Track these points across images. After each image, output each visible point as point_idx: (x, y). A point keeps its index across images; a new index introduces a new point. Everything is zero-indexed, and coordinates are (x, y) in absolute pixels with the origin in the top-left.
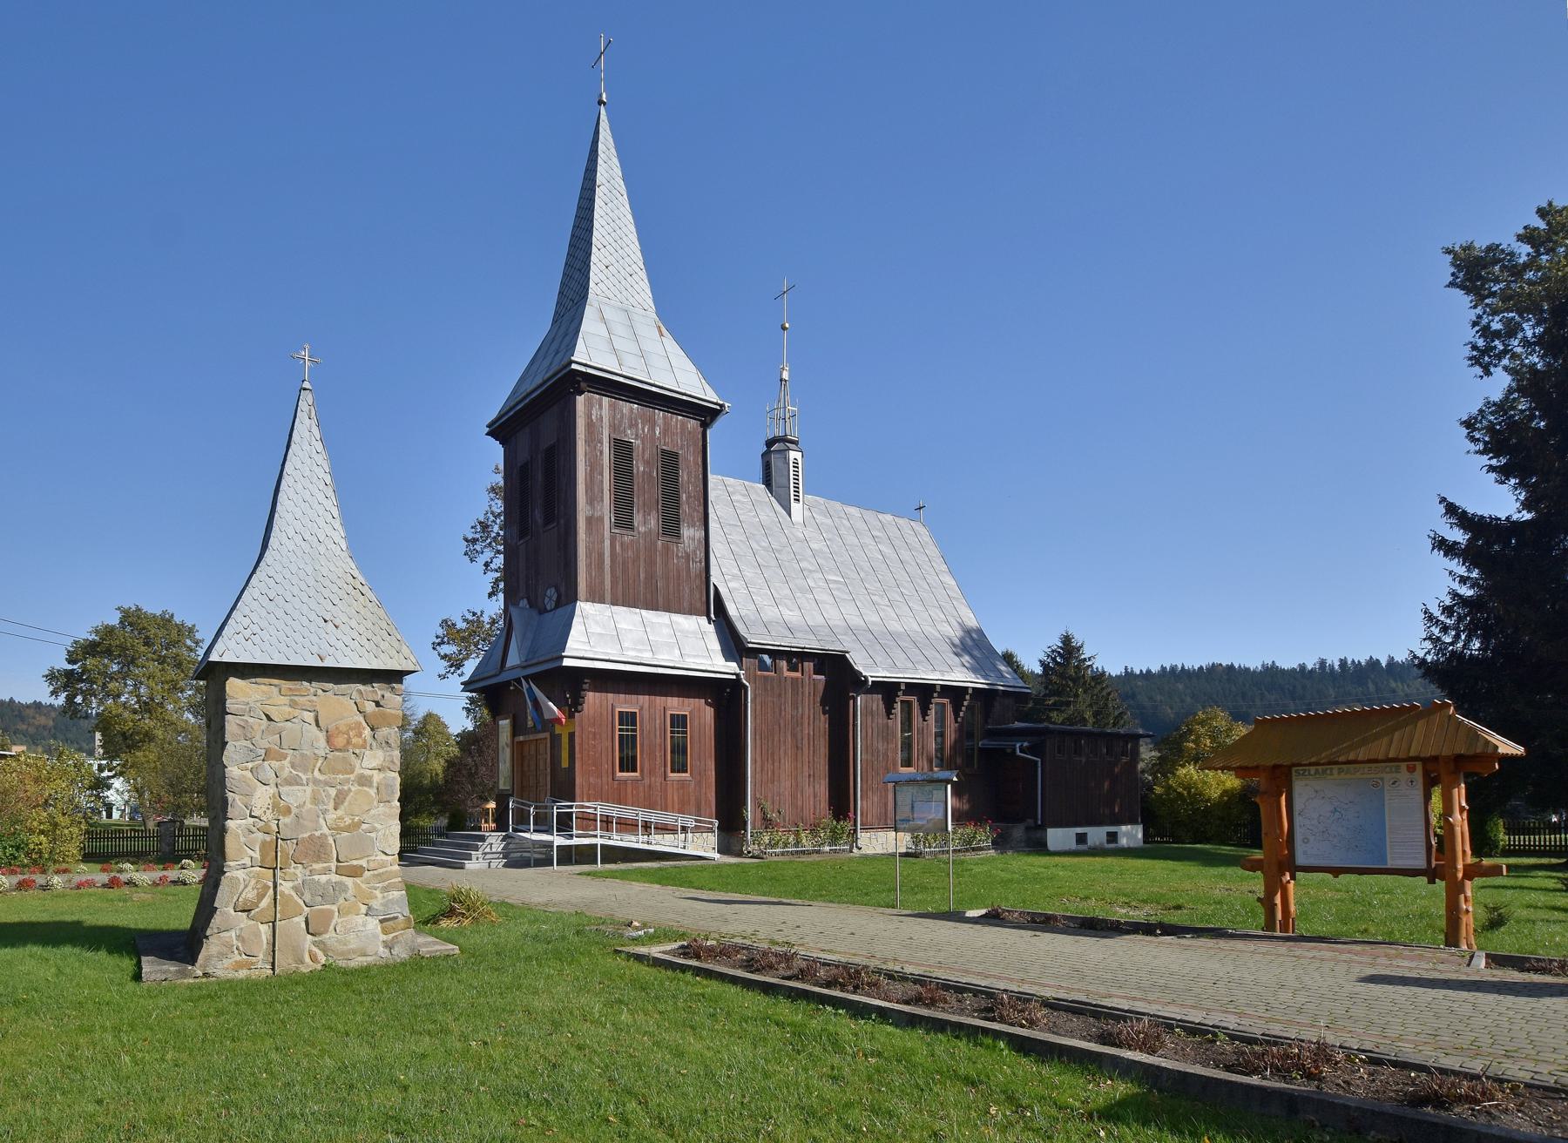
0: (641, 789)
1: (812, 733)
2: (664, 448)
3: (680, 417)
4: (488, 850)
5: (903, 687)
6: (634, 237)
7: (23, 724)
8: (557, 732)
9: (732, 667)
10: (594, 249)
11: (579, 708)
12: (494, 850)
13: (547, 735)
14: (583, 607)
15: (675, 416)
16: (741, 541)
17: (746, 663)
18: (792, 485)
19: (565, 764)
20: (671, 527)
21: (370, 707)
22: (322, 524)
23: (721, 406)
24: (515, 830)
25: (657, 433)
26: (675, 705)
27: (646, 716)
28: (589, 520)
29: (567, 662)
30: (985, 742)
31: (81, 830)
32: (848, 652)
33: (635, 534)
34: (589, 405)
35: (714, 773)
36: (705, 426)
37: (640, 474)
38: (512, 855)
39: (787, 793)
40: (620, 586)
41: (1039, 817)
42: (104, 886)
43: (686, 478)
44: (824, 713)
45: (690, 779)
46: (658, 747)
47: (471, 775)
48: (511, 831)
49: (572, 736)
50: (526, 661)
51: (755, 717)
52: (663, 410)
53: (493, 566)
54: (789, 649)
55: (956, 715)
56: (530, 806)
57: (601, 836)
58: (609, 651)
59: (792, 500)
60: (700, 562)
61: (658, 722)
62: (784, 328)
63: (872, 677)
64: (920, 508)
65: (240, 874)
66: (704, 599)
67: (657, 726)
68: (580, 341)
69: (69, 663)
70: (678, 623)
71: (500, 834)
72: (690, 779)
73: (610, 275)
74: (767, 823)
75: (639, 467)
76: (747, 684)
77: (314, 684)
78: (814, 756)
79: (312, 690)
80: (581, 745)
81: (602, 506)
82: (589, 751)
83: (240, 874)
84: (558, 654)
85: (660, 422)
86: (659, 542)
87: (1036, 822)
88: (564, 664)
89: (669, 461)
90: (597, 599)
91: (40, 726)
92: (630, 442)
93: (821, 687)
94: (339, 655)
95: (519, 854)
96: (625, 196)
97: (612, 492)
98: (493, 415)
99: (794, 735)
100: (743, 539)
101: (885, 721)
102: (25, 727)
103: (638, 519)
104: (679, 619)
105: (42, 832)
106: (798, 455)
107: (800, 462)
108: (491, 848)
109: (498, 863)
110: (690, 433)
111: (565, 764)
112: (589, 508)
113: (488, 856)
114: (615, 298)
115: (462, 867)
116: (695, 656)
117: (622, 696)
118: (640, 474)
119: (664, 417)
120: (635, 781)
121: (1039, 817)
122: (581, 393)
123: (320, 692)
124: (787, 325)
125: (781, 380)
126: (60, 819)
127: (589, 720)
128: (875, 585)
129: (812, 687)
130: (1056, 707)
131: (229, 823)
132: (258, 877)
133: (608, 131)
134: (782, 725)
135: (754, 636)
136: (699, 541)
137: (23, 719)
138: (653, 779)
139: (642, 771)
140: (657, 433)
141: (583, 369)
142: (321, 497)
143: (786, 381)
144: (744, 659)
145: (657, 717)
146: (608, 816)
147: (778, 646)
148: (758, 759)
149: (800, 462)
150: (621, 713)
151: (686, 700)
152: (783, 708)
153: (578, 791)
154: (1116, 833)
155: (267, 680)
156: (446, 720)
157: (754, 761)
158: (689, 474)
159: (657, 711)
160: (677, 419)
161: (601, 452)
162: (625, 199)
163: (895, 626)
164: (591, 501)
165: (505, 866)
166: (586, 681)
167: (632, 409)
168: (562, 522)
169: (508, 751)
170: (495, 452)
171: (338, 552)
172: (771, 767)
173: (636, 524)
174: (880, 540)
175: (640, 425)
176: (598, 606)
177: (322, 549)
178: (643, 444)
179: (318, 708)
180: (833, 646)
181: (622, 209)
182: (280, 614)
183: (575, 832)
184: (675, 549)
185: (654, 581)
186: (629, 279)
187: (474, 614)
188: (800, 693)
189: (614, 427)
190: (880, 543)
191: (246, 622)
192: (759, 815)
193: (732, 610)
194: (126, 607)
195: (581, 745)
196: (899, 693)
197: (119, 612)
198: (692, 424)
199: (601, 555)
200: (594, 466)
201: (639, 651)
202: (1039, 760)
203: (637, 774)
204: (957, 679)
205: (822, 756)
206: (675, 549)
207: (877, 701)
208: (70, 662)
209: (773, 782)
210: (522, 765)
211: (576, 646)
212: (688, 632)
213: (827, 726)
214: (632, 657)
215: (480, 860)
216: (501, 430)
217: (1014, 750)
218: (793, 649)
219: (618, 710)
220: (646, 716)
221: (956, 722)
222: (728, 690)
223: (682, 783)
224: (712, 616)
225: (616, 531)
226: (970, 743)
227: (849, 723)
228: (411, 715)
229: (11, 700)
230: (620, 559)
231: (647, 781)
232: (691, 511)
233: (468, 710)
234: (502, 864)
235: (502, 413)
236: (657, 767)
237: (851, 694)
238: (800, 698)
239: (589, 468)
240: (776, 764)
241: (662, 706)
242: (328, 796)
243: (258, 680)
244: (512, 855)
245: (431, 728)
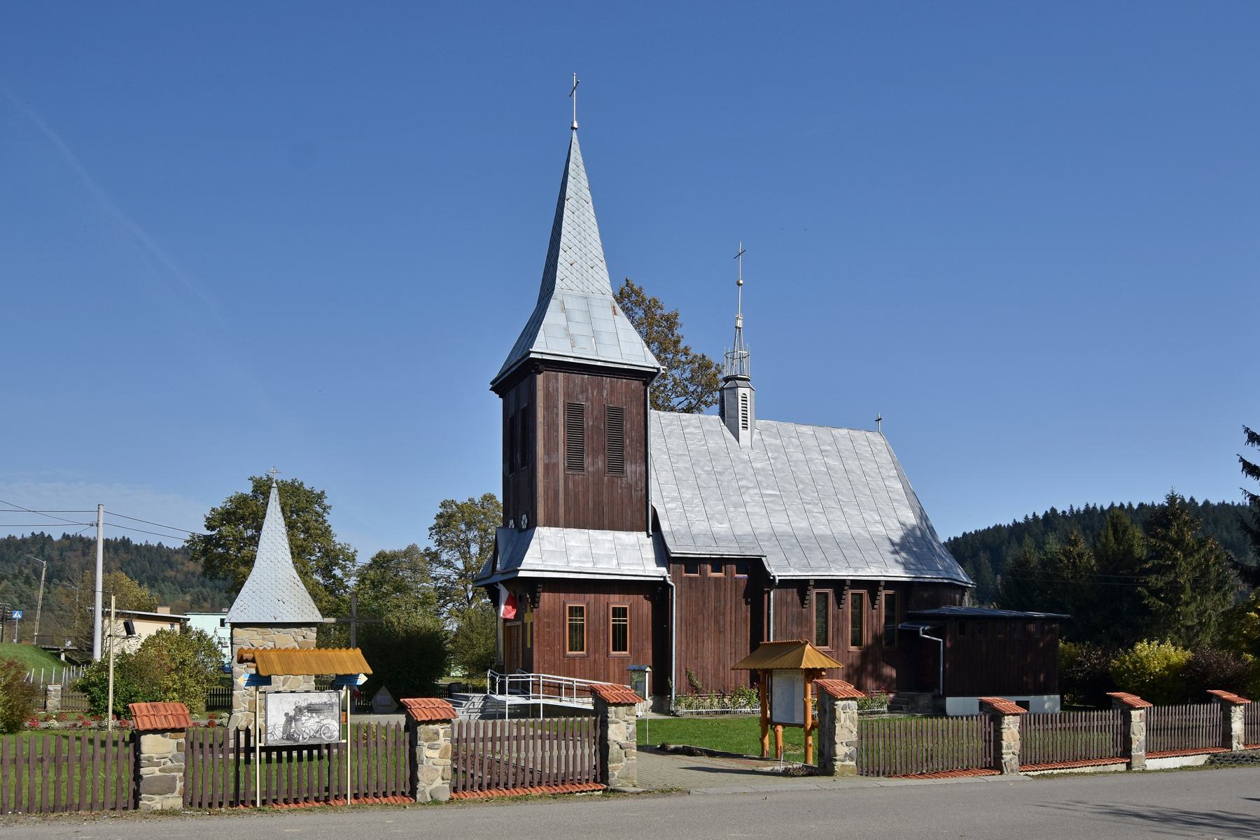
0: (587, 663)
1: (733, 619)
2: (610, 405)
3: (624, 380)
5: (812, 583)
6: (596, 236)
7: (172, 570)
10: (561, 252)
11: (536, 605)
12: (476, 707)
14: (541, 531)
15: (620, 380)
16: (686, 468)
17: (673, 568)
18: (740, 415)
19: (529, 646)
20: (616, 467)
21: (300, 639)
22: (279, 552)
23: (658, 369)
25: (605, 395)
26: (616, 601)
27: (592, 609)
28: (547, 467)
29: (521, 574)
30: (904, 624)
31: (203, 688)
32: (765, 556)
34: (547, 380)
35: (650, 652)
36: (646, 384)
37: (590, 427)
39: (709, 666)
40: (572, 514)
41: (941, 688)
42: (205, 726)
43: (629, 426)
44: (747, 603)
45: (629, 655)
46: (601, 632)
50: (505, 569)
51: (680, 608)
52: (610, 377)
54: (709, 556)
57: (543, 698)
58: (557, 564)
59: (740, 428)
60: (641, 490)
61: (602, 613)
62: (739, 284)
63: (778, 576)
64: (879, 420)
65: (239, 715)
66: (644, 518)
67: (601, 616)
68: (541, 332)
69: (208, 529)
70: (620, 539)
71: (480, 695)
72: (629, 655)
73: (574, 271)
74: (694, 689)
75: (589, 422)
76: (673, 584)
77: (273, 629)
78: (735, 638)
79: (273, 632)
81: (558, 455)
83: (239, 715)
84: (515, 568)
85: (608, 386)
86: (606, 478)
88: (519, 575)
89: (615, 416)
90: (553, 524)
91: (188, 572)
93: (743, 585)
94: (284, 617)
96: (591, 203)
97: (566, 444)
98: (495, 375)
99: (717, 622)
100: (688, 466)
101: (799, 609)
102: (173, 573)
103: (587, 461)
104: (622, 535)
105: (175, 690)
106: (747, 391)
110: (633, 391)
111: (529, 646)
112: (546, 457)
114: (577, 289)
116: (629, 564)
117: (572, 595)
118: (590, 427)
119: (611, 382)
120: (582, 657)
121: (941, 688)
122: (540, 373)
123: (276, 633)
124: (741, 282)
125: (736, 327)
126: (187, 680)
127: (544, 614)
128: (812, 494)
129: (734, 584)
130: (1157, 570)
131: (234, 692)
132: (247, 715)
133: (579, 152)
134: (706, 615)
135: (675, 549)
136: (641, 474)
137: (171, 566)
138: (597, 656)
139: (588, 650)
140: (605, 395)
141: (539, 356)
142: (280, 540)
143: (740, 328)
144: (671, 565)
145: (601, 610)
147: (699, 554)
148: (684, 640)
150: (571, 608)
151: (626, 596)
152: (706, 601)
153: (535, 665)
154: (1028, 702)
155: (250, 628)
157: (679, 643)
158: (632, 424)
159: (601, 605)
160: (622, 383)
161: (557, 415)
162: (590, 208)
163: (821, 529)
164: (548, 452)
166: (539, 586)
167: (583, 379)
168: (530, 466)
170: (497, 402)
171: (288, 565)
173: (585, 466)
174: (827, 453)
175: (590, 391)
176: (553, 529)
177: (280, 565)
178: (592, 404)
179: (275, 640)
181: (587, 214)
182: (257, 598)
183: (531, 694)
184: (619, 482)
185: (601, 508)
186: (590, 271)
188: (723, 589)
189: (567, 394)
190: (827, 456)
191: (242, 603)
192: (685, 680)
193: (664, 526)
194: (258, 477)
195: (538, 632)
196: (809, 588)
197: (251, 481)
198: (636, 384)
199: (556, 492)
200: (551, 426)
201: (583, 562)
202: (941, 640)
203: (584, 653)
204: (868, 574)
206: (619, 482)
207: (792, 595)
208: (209, 527)
209: (697, 658)
210: (511, 644)
212: (627, 545)
213: (749, 614)
214: (575, 568)
215: (465, 713)
216: (500, 387)
217: (918, 632)
218: (712, 556)
219: (568, 605)
220: (592, 609)
223: (622, 659)
224: (650, 531)
225: (569, 473)
226: (893, 625)
227: (764, 612)
229: (160, 545)
230: (572, 493)
231: (592, 658)
232: (633, 451)
234: (478, 717)
235: (503, 371)
236: (601, 647)
237: (765, 589)
238: (722, 594)
239: (546, 428)
240: (700, 644)
241: (606, 601)
242: (280, 680)
243: (248, 629)
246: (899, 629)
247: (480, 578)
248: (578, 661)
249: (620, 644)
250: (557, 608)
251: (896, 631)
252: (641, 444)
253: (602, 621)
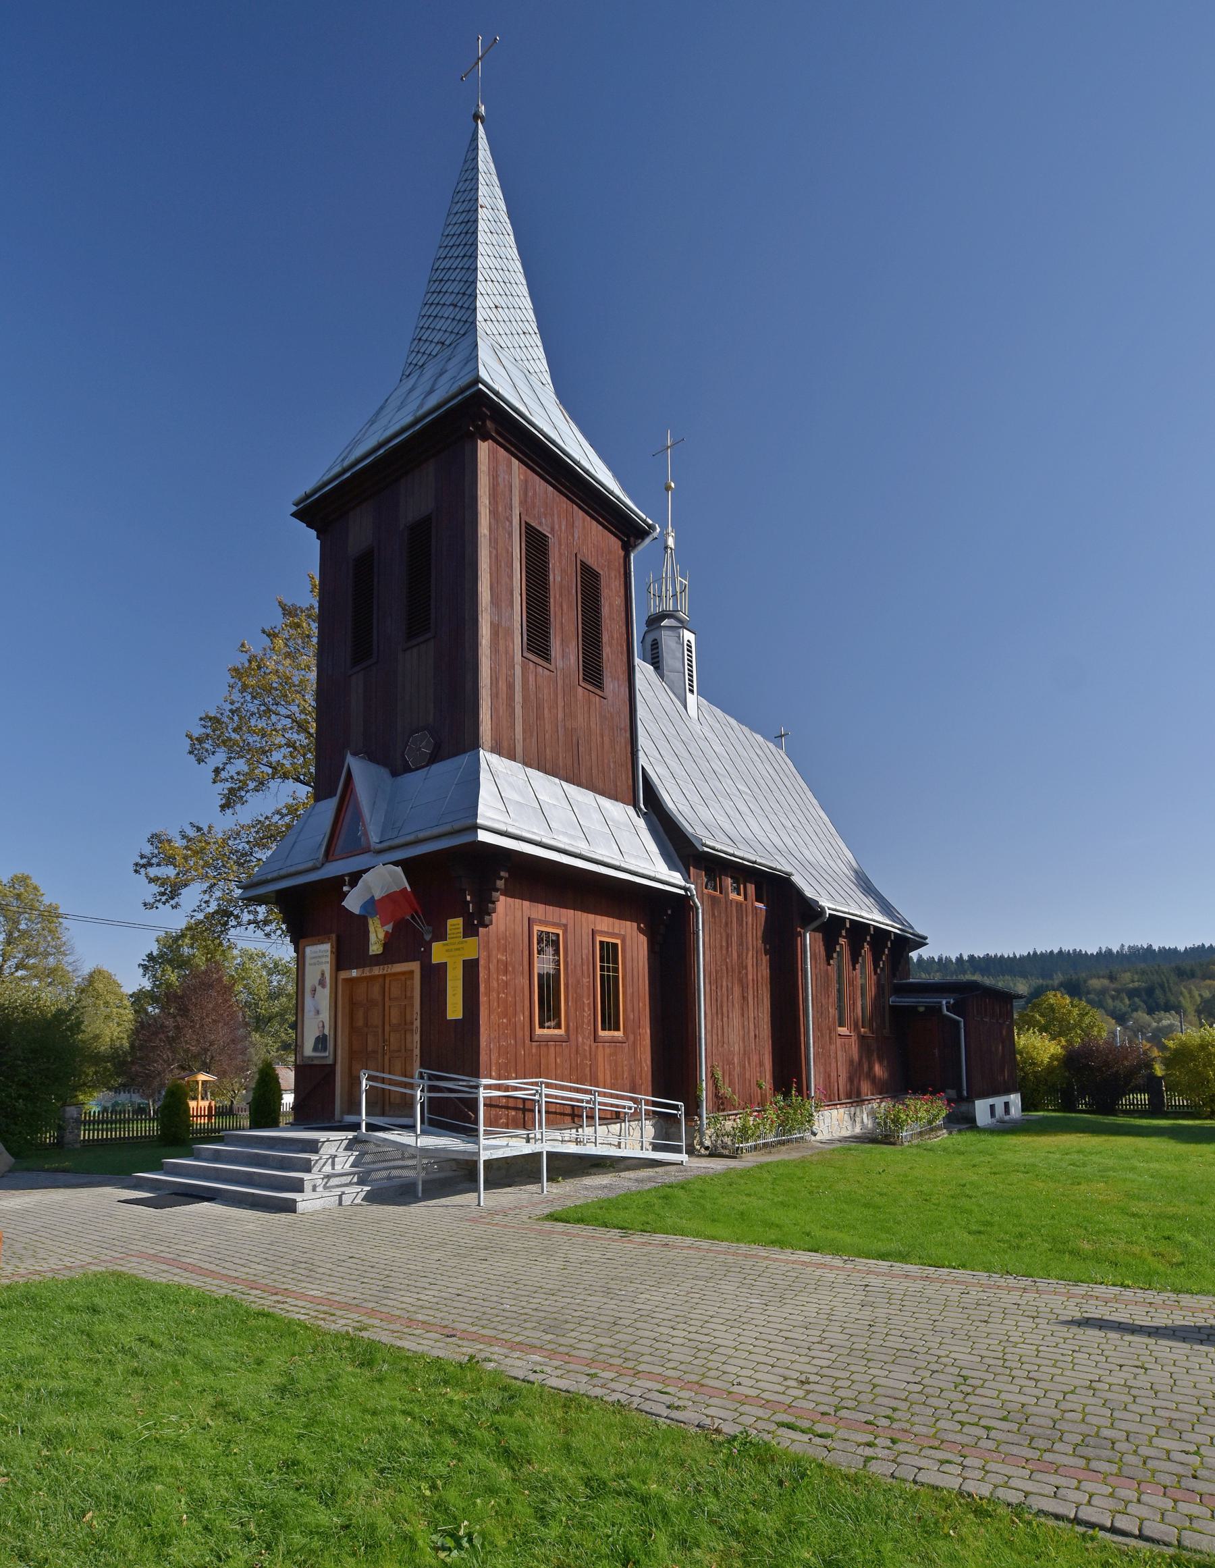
4: (328, 1169)
8: (435, 960)
9: (677, 878)
13: (415, 966)
19: (455, 1010)
24: (371, 1127)
28: (495, 629)
33: (552, 667)
35: (648, 1031)
36: (627, 548)
38: (374, 1176)
47: (171, 1041)
48: (364, 1130)
49: (471, 968)
53: (224, 775)
55: (876, 965)
56: (411, 1086)
80: (488, 981)
82: (498, 993)
87: (959, 1091)
92: (546, 536)
95: (384, 1174)
107: (693, 645)
108: (333, 1164)
109: (355, 1193)
111: (455, 1010)
113: (334, 1181)
115: (289, 1207)
127: (498, 941)
146: (573, 1106)
149: (693, 645)
156: (119, 979)
165: (370, 1198)
166: (503, 874)
169: (325, 994)
170: (308, 541)
172: (720, 1023)
180: (782, 864)
187: (199, 829)
203: (561, 1032)
205: (765, 1011)
211: (490, 814)
221: (876, 973)
222: (669, 912)
228: (74, 971)
233: (145, 968)
240: (725, 1019)
244: (374, 1176)
245: (100, 986)
246: (890, 1006)
247: (255, 880)
248: (553, 1048)
249: (610, 1021)
250: (519, 930)
251: (887, 1007)
252: (622, 647)
253: (585, 968)
